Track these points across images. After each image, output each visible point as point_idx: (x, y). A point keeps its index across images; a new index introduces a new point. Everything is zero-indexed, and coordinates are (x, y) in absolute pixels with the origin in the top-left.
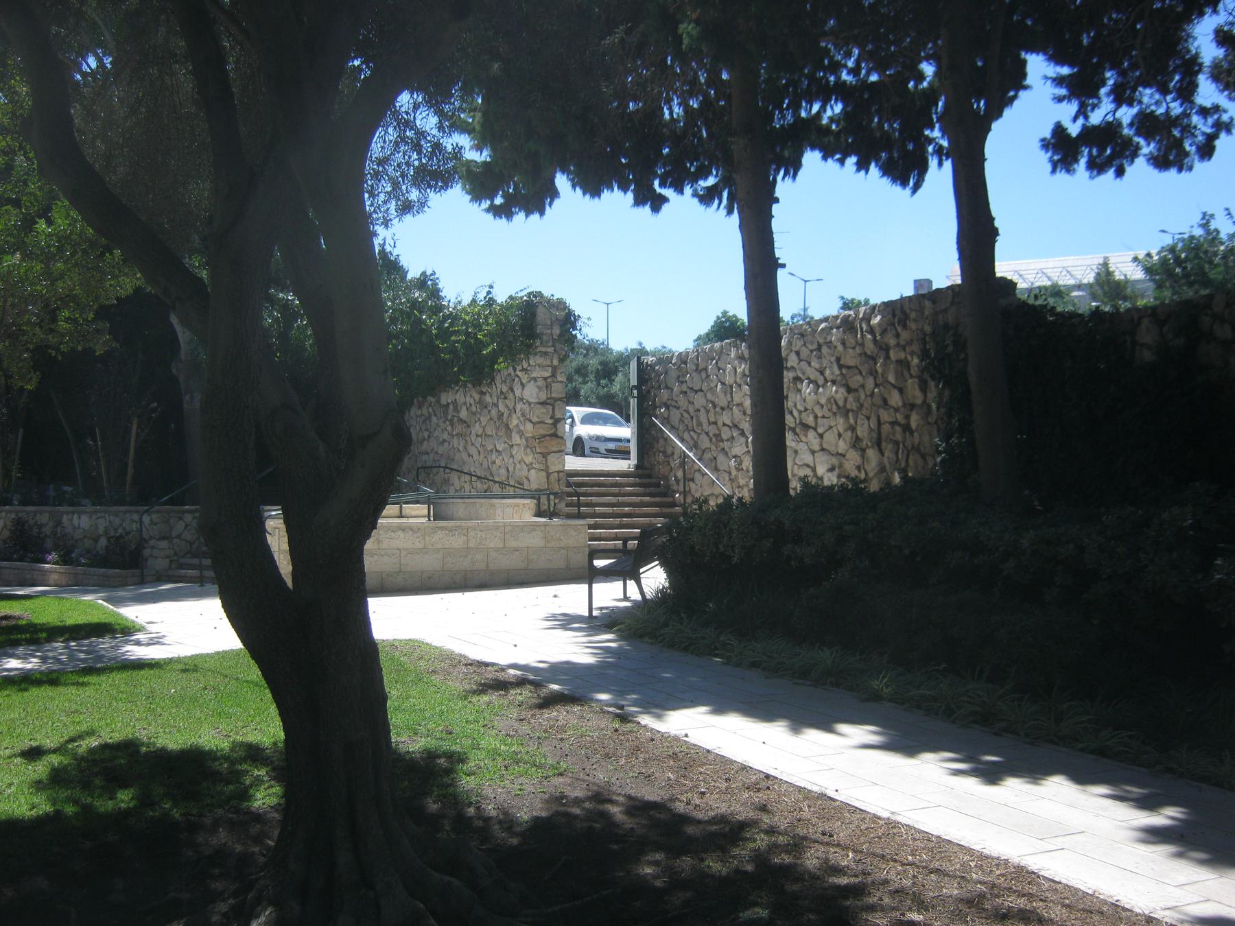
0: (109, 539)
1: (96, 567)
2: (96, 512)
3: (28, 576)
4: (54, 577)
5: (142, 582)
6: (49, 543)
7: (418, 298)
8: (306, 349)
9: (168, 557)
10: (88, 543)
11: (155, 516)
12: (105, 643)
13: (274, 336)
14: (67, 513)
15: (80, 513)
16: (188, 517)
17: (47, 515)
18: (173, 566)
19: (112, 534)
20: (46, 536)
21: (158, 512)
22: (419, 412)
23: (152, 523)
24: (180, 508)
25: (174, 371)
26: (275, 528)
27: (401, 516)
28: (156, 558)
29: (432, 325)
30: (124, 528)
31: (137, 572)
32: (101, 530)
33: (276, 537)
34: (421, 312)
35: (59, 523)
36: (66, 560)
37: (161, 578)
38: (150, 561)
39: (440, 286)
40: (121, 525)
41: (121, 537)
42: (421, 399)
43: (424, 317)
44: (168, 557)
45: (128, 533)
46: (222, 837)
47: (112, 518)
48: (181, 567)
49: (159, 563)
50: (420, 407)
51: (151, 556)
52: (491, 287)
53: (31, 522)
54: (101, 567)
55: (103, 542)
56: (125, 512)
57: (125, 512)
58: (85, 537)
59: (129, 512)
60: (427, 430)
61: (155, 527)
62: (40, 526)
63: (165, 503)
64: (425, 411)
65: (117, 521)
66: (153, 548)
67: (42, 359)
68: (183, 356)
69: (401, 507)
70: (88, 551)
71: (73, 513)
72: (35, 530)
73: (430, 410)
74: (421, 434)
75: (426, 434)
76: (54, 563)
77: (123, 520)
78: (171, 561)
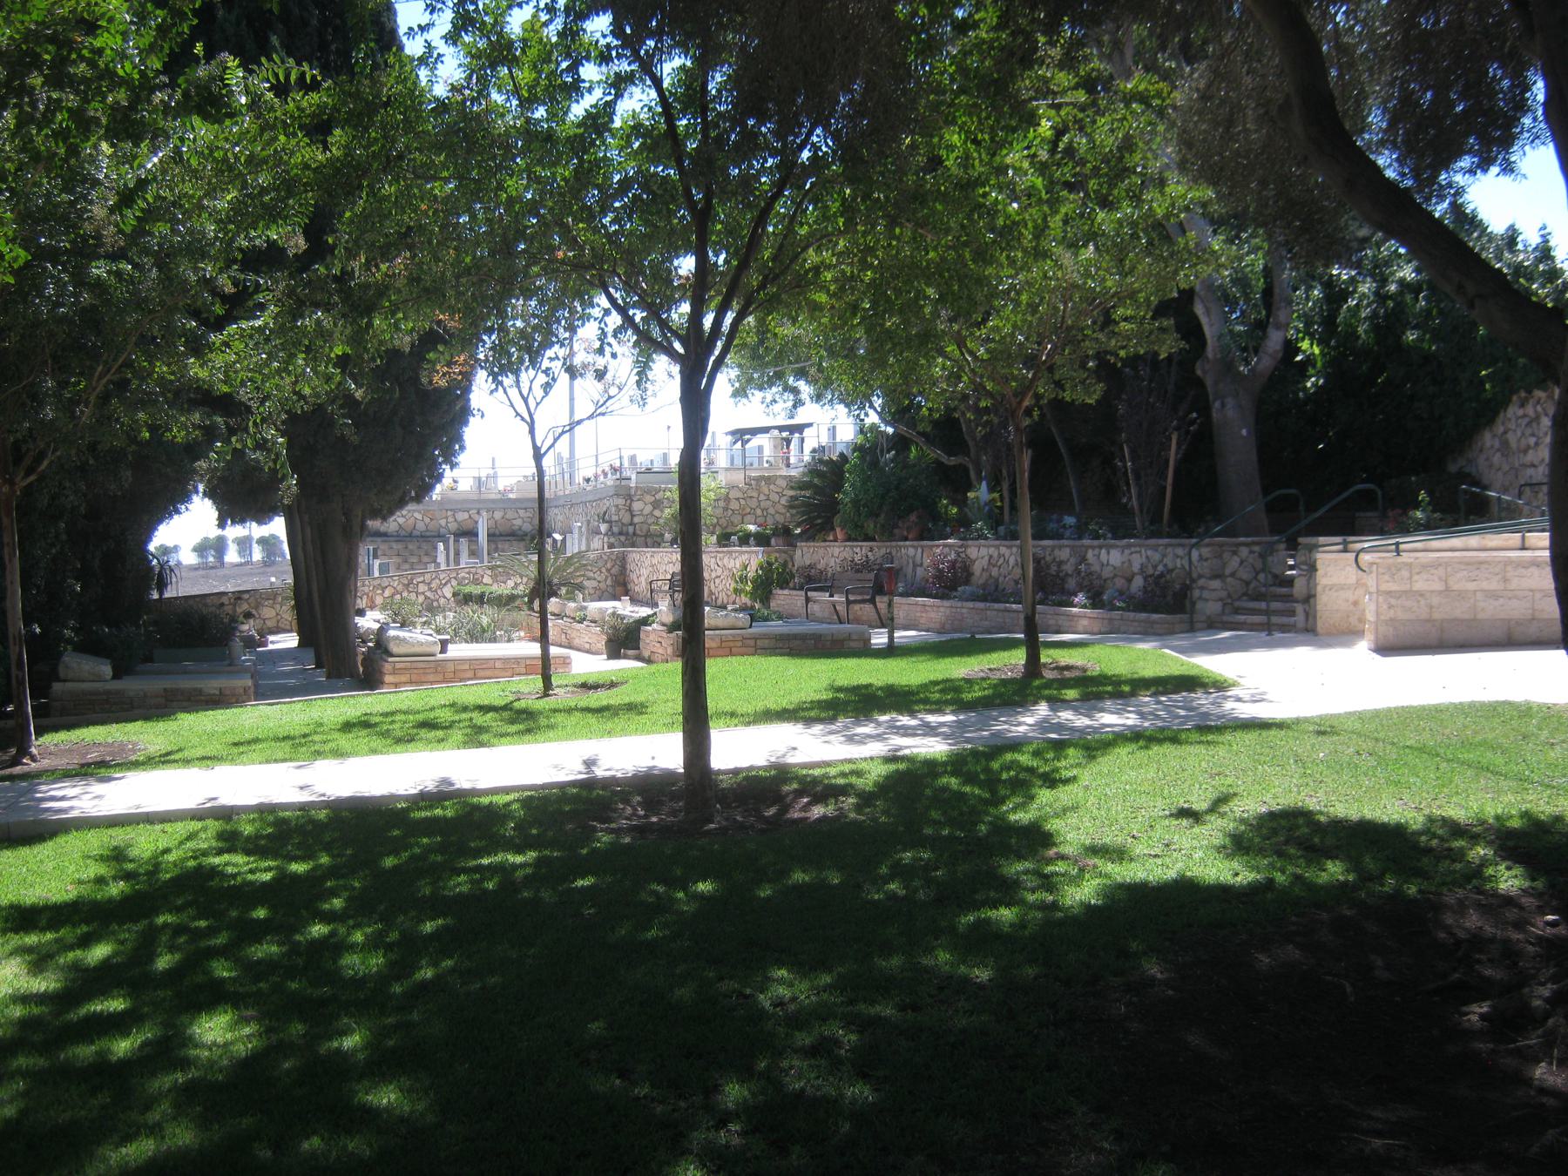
0: (1145, 579)
1: (1133, 611)
2: (1129, 546)
3: (1051, 622)
4: (1085, 622)
5: (1192, 628)
6: (1071, 583)
7: (1523, 261)
8: (1358, 337)
9: (1221, 600)
10: (1120, 583)
11: (1205, 551)
12: (1202, 700)
13: (1316, 323)
14: (1093, 547)
15: (1109, 548)
16: (1244, 551)
17: (1068, 550)
18: (1227, 611)
19: (1150, 571)
20: (1067, 575)
21: (1208, 545)
22: (1520, 412)
23: (1201, 558)
24: (1234, 540)
25: (1199, 372)
26: (1372, 564)
27: (1523, 548)
28: (1207, 600)
29: (1547, 297)
30: (1165, 565)
31: (1185, 617)
32: (1136, 567)
33: (1374, 575)
34: (1531, 279)
35: (1083, 559)
36: (1096, 601)
37: (1213, 625)
38: (1199, 606)
39: (1552, 244)
40: (1161, 561)
41: (1162, 575)
42: (1523, 394)
43: (1534, 286)
44: (1221, 600)
45: (1170, 571)
46: (1473, 920)
47: (1150, 553)
48: (1237, 611)
49: (1211, 608)
50: (1522, 405)
51: (1200, 598)
52: (1544, 228)
53: (1048, 558)
54: (1141, 611)
55: (1138, 582)
56: (1166, 546)
57: (1166, 546)
58: (1115, 576)
59: (1171, 545)
60: (1533, 435)
61: (1205, 564)
62: (1061, 563)
63: (1218, 534)
64: (1530, 410)
65: (1156, 557)
66: (1202, 588)
67: (1107, 370)
68: (1210, 352)
69: (1523, 537)
70: (1121, 593)
71: (1100, 547)
72: (1054, 568)
73: (1539, 408)
74: (1523, 441)
75: (1532, 441)
76: (1084, 607)
77: (1164, 556)
78: (1225, 604)
